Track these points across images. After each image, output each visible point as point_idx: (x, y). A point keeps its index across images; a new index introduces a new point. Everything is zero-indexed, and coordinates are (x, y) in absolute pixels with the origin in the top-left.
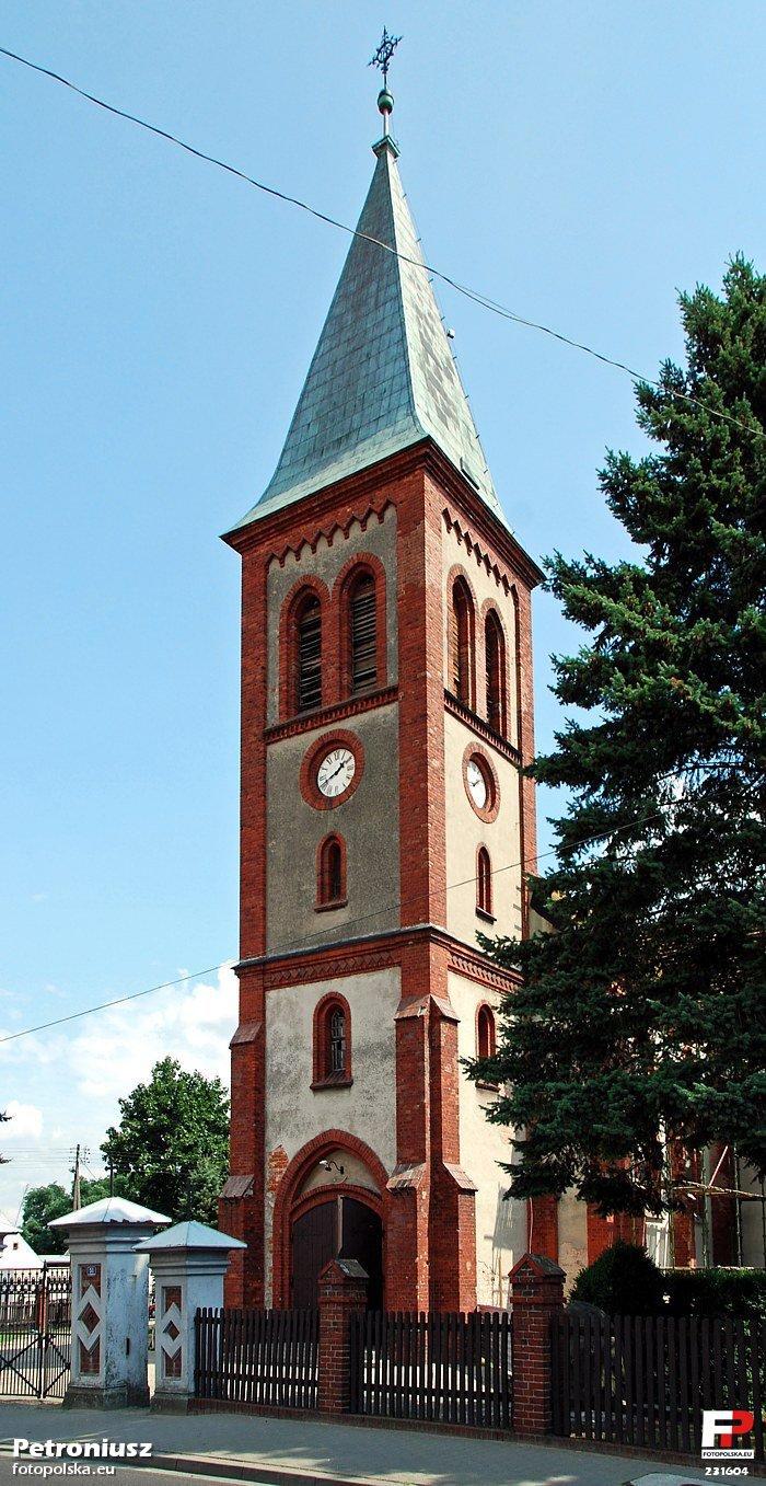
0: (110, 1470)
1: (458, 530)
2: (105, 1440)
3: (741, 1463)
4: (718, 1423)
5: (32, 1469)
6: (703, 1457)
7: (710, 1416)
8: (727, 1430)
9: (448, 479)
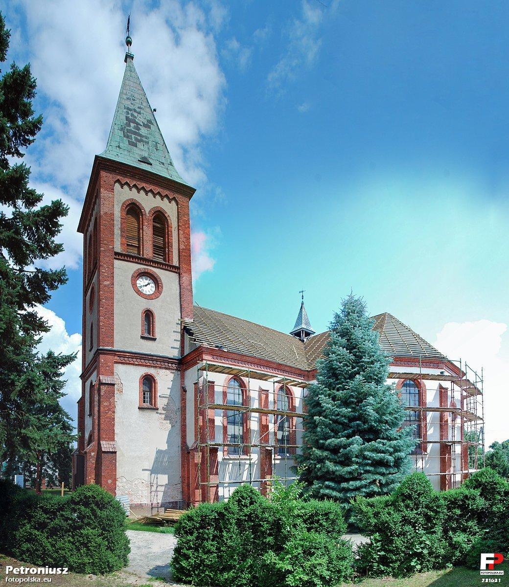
0: (49, 580)
1: (128, 185)
2: (47, 567)
3: (497, 577)
4: (487, 559)
5: (15, 580)
6: (481, 574)
7: (484, 556)
8: (492, 562)
9: (116, 167)
